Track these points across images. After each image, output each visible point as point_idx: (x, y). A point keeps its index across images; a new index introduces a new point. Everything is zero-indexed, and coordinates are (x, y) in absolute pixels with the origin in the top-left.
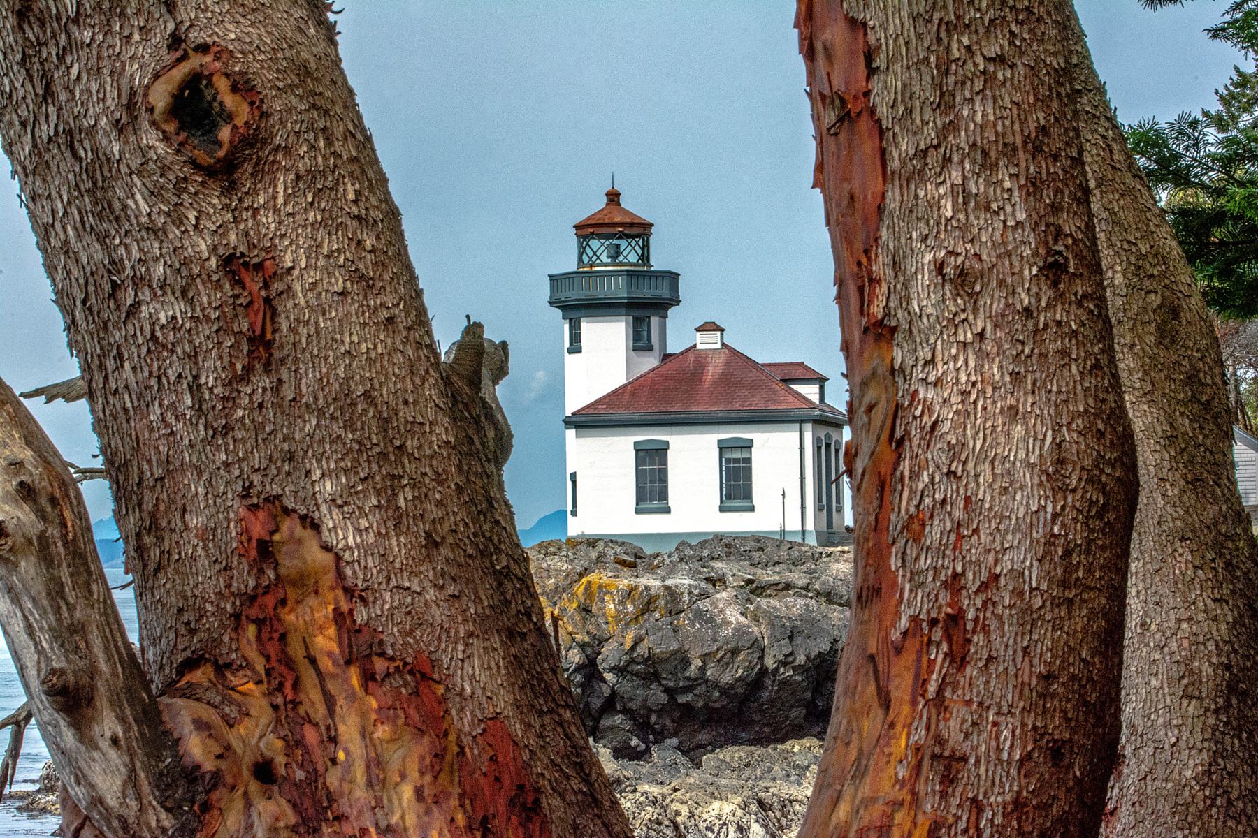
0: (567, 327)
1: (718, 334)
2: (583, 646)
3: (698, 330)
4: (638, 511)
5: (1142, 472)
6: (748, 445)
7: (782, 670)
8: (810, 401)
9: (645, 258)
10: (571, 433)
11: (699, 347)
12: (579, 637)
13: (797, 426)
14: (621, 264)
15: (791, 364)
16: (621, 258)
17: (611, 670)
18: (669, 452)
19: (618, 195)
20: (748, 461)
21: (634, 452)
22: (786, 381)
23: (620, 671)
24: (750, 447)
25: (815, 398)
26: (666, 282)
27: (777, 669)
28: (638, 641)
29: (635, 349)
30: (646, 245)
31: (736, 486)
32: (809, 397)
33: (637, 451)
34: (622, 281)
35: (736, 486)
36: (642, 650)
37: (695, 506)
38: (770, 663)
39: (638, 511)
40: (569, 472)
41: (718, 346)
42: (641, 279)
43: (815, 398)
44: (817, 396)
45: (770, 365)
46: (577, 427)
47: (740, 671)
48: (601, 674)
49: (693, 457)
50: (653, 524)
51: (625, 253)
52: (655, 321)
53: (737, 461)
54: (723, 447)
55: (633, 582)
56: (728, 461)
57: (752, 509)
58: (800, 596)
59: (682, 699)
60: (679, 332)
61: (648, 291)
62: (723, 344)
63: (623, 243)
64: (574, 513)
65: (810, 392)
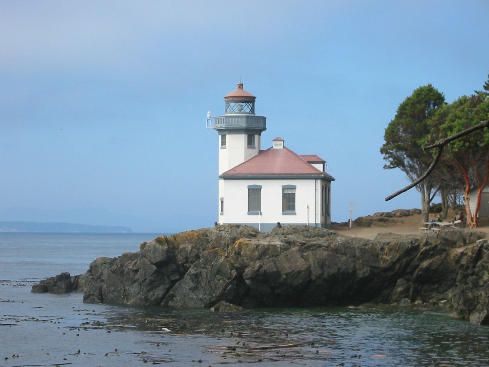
0: (220, 137)
1: (282, 142)
2: (237, 269)
3: (274, 141)
4: (249, 214)
5: (6, 231)
6: (294, 188)
7: (318, 281)
8: (321, 172)
9: (252, 110)
10: (222, 182)
11: (274, 147)
12: (236, 265)
13: (315, 180)
14: (243, 113)
15: (237, 167)
16: (243, 111)
17: (248, 279)
18: (262, 190)
19: (242, 85)
20: (294, 194)
21: (248, 190)
22: (310, 162)
23: (252, 279)
24: (295, 189)
25: (321, 169)
26: (262, 120)
27: (316, 280)
28: (260, 267)
29: (248, 148)
30: (253, 105)
31: (289, 203)
32: (319, 169)
33: (249, 189)
34: (244, 120)
35: (289, 203)
36: (262, 270)
37: (271, 213)
38: (313, 278)
39: (249, 214)
40: (220, 197)
41: (282, 147)
42: (251, 119)
43: (321, 169)
44: (322, 169)
45: (303, 156)
46: (224, 179)
47: (301, 281)
48: (244, 281)
49: (272, 192)
50: (288, 220)
51: (244, 109)
52: (256, 137)
53: (289, 194)
54: (284, 188)
55: (257, 242)
56: (286, 194)
57: (295, 214)
58: (325, 250)
59: (276, 292)
60: (265, 140)
61: (254, 125)
62: (284, 147)
63: (244, 104)
64: (222, 214)
65: (319, 167)
